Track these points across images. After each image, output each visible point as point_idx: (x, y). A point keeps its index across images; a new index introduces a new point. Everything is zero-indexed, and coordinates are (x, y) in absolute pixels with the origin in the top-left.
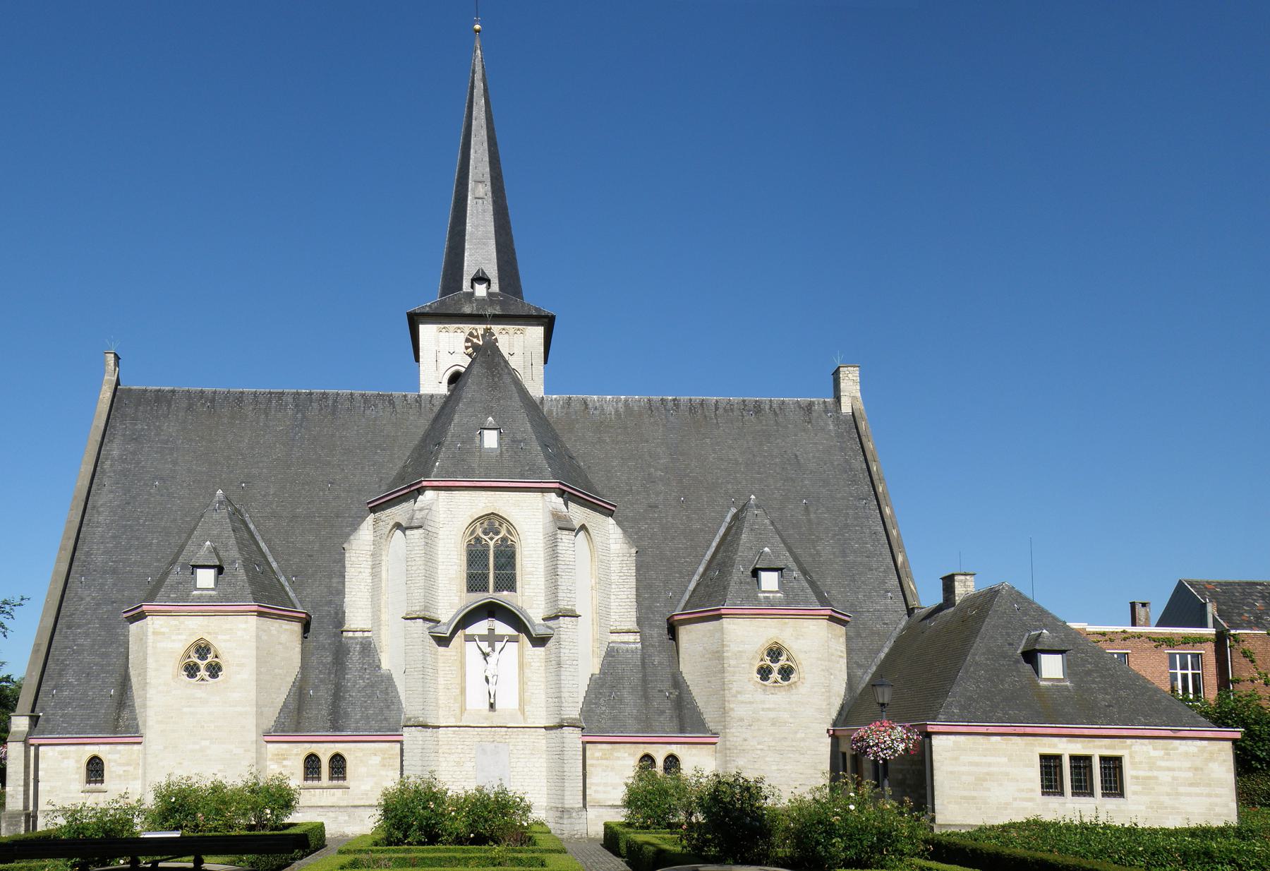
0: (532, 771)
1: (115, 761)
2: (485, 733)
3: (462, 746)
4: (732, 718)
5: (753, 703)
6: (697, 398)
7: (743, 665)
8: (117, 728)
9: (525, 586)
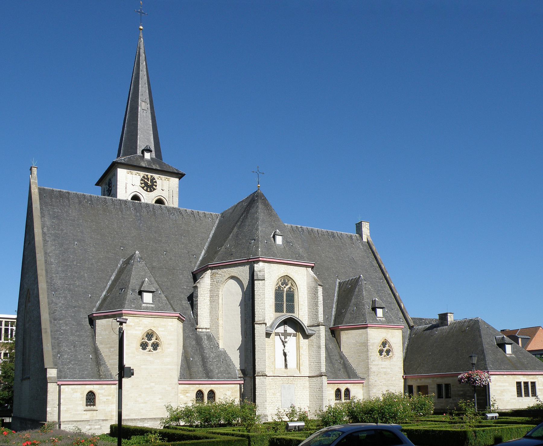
0: (303, 397)
1: (102, 394)
2: (285, 379)
3: (275, 386)
4: (371, 372)
5: (378, 365)
6: (310, 228)
7: (375, 349)
8: (100, 376)
9: (300, 311)
